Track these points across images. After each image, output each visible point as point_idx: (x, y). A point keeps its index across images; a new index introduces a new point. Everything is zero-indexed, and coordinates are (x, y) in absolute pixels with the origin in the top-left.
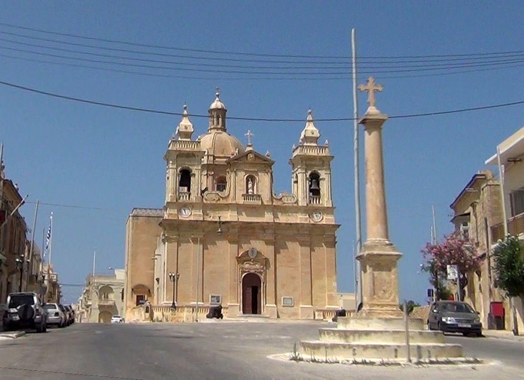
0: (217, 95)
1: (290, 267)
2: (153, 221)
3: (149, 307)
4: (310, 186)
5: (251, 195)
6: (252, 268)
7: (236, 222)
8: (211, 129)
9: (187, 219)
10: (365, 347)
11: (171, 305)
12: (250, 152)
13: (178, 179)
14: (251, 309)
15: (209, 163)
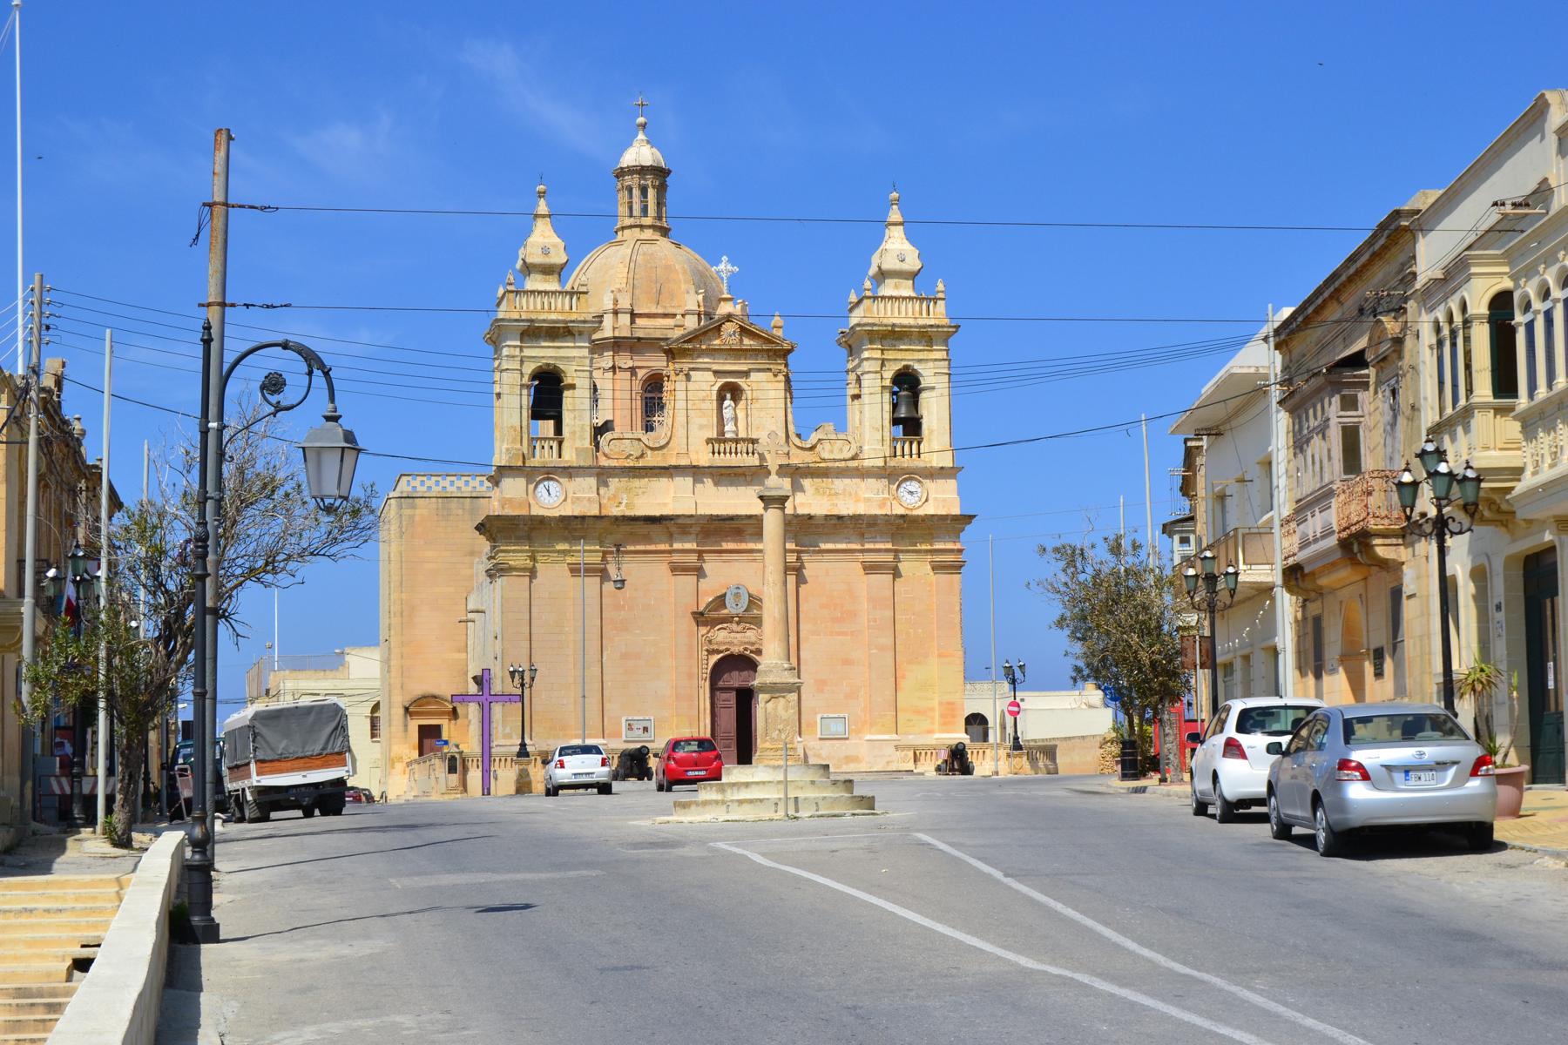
0: (639, 125)
1: (839, 634)
2: (460, 512)
3: (457, 756)
4: (895, 406)
5: (731, 440)
6: (735, 641)
7: (692, 516)
8: (623, 228)
9: (556, 513)
10: (741, 802)
11: (517, 749)
12: (729, 318)
13: (527, 400)
14: (734, 749)
15: (617, 334)
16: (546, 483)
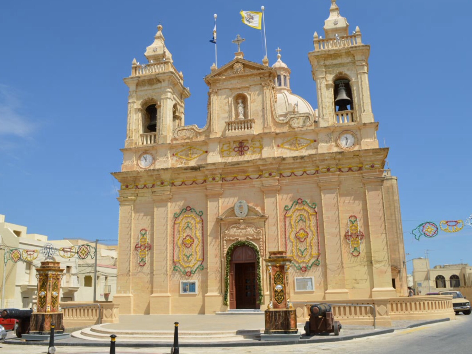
16: (145, 156)
